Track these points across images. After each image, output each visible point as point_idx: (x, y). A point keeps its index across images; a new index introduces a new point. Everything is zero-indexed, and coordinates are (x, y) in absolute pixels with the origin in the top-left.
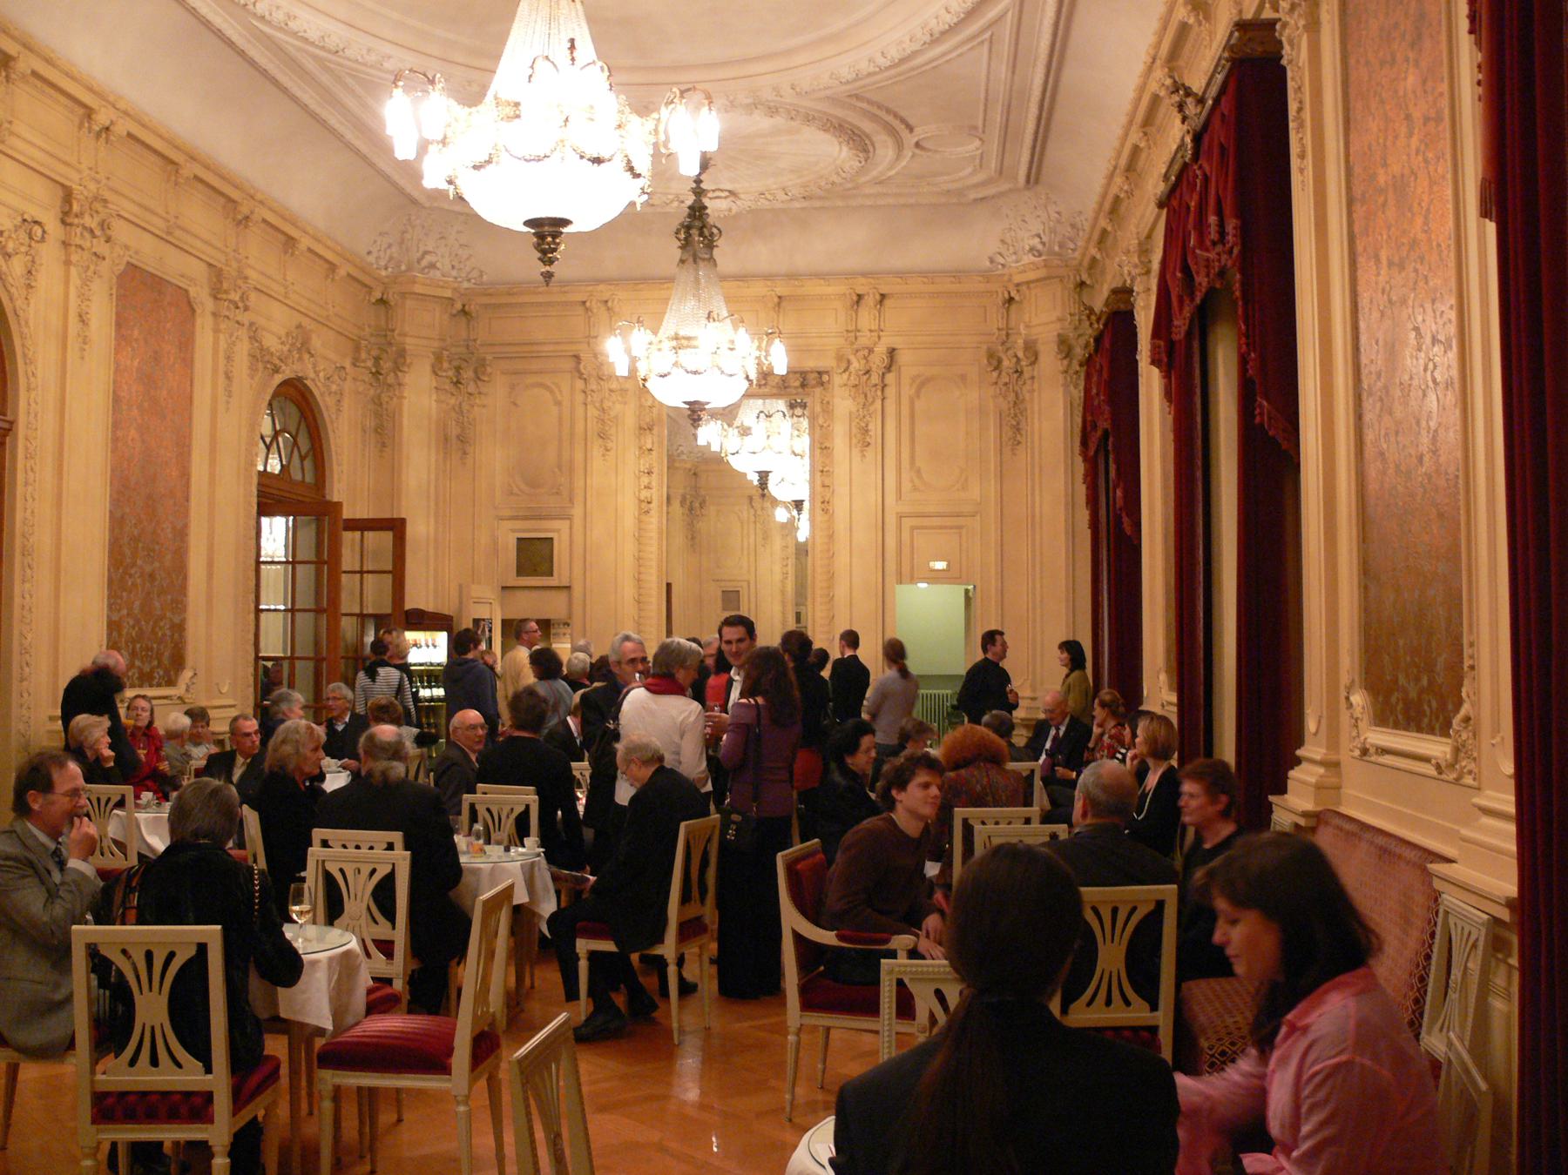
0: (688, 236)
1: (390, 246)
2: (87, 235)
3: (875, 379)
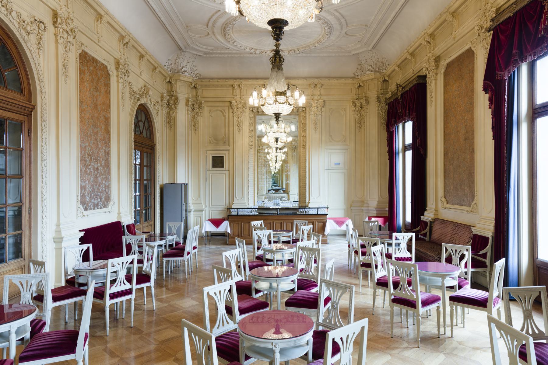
0: (276, 60)
1: (171, 64)
2: (65, 33)
3: (319, 109)
